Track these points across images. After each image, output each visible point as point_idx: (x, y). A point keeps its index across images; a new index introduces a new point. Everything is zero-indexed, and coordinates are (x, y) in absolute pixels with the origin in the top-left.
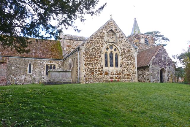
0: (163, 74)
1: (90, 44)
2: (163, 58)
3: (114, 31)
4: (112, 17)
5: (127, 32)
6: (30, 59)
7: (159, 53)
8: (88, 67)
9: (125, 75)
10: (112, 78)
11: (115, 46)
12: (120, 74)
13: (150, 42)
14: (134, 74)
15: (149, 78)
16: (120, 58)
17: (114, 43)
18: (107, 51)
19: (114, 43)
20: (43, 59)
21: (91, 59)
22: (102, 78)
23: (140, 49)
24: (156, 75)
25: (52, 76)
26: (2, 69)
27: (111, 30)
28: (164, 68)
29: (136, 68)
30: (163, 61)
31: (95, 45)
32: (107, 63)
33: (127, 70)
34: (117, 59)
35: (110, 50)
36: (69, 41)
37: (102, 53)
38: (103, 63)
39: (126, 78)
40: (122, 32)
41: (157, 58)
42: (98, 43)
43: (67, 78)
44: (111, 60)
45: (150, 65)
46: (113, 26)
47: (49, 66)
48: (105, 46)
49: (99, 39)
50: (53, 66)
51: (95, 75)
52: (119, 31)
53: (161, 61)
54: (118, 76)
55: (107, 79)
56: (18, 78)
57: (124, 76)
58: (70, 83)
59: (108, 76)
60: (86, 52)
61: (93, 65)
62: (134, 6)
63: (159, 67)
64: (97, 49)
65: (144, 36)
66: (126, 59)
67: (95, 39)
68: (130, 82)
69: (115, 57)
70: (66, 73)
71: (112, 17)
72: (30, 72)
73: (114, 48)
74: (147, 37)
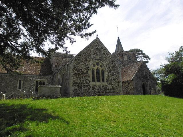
0: (146, 88)
4: (98, 37)
7: (141, 68)
9: (111, 89)
14: (119, 88)
16: (106, 74)
19: (100, 60)
21: (80, 75)
24: (139, 88)
27: (97, 48)
32: (94, 79)
34: (103, 74)
35: (96, 67)
38: (90, 79)
46: (99, 45)
48: (91, 63)
51: (82, 89)
61: (81, 80)
65: (126, 54)
72: (20, 88)
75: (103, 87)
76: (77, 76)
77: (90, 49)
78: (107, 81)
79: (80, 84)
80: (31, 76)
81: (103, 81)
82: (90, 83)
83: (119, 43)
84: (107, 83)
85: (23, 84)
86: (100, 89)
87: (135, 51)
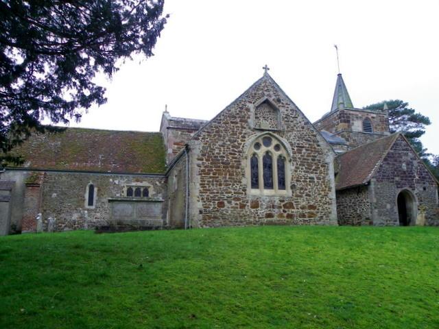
0: (409, 205)
1: (215, 135)
2: (404, 164)
3: (274, 103)
4: (268, 72)
5: (314, 105)
6: (91, 174)
7: (392, 151)
8: (209, 190)
9: (303, 208)
10: (269, 216)
11: (276, 138)
12: (290, 206)
13: (376, 128)
14: (326, 206)
15: (370, 214)
16: (289, 168)
17: (274, 131)
18: (256, 151)
19: (274, 131)
20: (119, 175)
21: (218, 170)
22: (245, 216)
23: (351, 145)
24: (389, 206)
25: (115, 212)
26: (29, 198)
27: (267, 102)
28: (410, 189)
29: (333, 190)
30: (404, 172)
31: (227, 138)
32: (257, 181)
33: (310, 196)
34: (281, 169)
35: (263, 149)
36: (180, 133)
37: (244, 156)
38: (247, 180)
39: (306, 214)
40: (294, 104)
41: (388, 164)
42: (234, 134)
43: (150, 217)
44: (269, 174)
45: (369, 183)
46: (271, 93)
47: (134, 189)
48: (250, 140)
49: (237, 123)
50: (142, 190)
51: (225, 208)
52: (287, 104)
53: (400, 173)
54: (286, 210)
55: (257, 219)
56: (65, 217)
57: (301, 210)
58: (157, 228)
59: (259, 212)
60: (203, 155)
61: (220, 185)
62: (336, 47)
63: (394, 187)
64: (230, 147)
65: (360, 115)
66: (306, 168)
67: (226, 123)
68: (316, 224)
69: (278, 166)
70: (150, 205)
71: (268, 72)
72: (91, 203)
73: (274, 142)
74: (370, 117)
75: (281, 201)
76: (211, 175)
77: (248, 104)
78: (293, 187)
79: (218, 193)
80: (59, 173)
81: (282, 184)
82: (245, 190)
83: (341, 85)
84: (293, 192)
85: (98, 195)
86: (273, 207)
87: (386, 107)
